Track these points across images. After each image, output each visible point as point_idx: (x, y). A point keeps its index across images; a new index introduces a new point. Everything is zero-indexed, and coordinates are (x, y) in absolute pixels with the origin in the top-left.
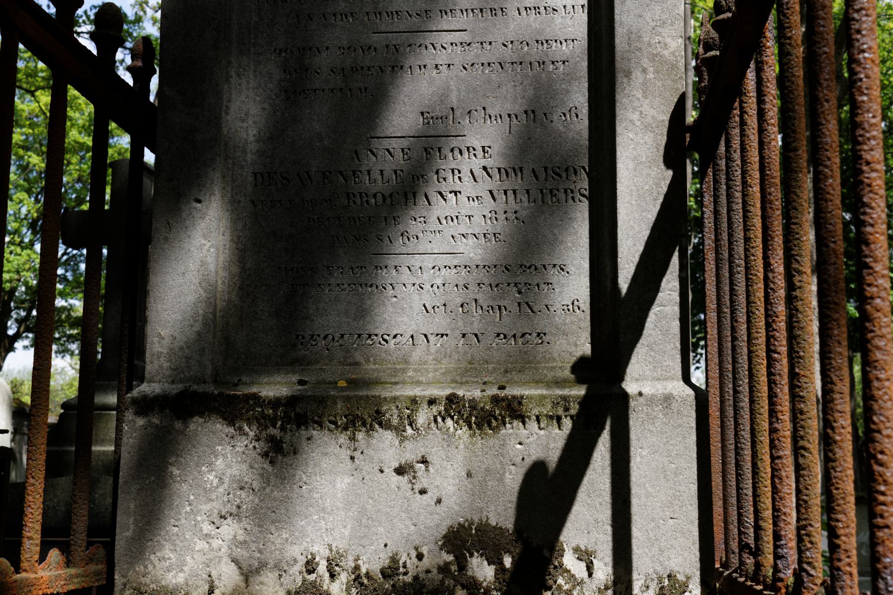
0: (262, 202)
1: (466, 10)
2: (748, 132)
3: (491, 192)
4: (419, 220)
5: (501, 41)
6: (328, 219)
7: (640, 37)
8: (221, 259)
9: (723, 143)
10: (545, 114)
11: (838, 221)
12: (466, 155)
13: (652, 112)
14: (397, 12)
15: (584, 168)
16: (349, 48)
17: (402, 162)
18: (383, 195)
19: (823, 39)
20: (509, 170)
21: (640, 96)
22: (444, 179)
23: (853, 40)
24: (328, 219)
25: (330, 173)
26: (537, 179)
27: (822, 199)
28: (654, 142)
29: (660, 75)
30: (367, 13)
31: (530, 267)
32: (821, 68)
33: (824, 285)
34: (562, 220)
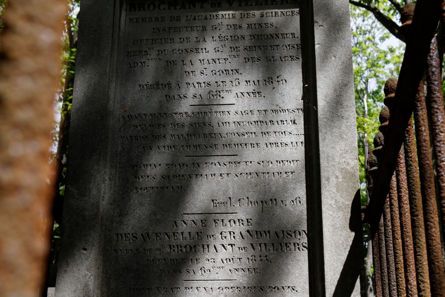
0: (121, 250)
1: (237, 144)
2: (394, 209)
3: (252, 245)
4: (210, 260)
5: (257, 161)
6: (159, 260)
7: (334, 159)
8: (97, 283)
9: (382, 217)
10: (282, 201)
11: (439, 250)
12: (237, 223)
13: (342, 200)
14: (199, 145)
15: (304, 231)
16: (172, 165)
17: (201, 228)
18: (190, 246)
19: (426, 157)
20: (262, 232)
21: (335, 191)
22: (225, 237)
23: (437, 156)
24: (159, 260)
25: (160, 234)
26: (278, 237)
27: (430, 239)
28: (343, 216)
29: (346, 180)
30: (183, 146)
31: (275, 288)
32: (426, 171)
33: (434, 285)
34: (293, 261)
